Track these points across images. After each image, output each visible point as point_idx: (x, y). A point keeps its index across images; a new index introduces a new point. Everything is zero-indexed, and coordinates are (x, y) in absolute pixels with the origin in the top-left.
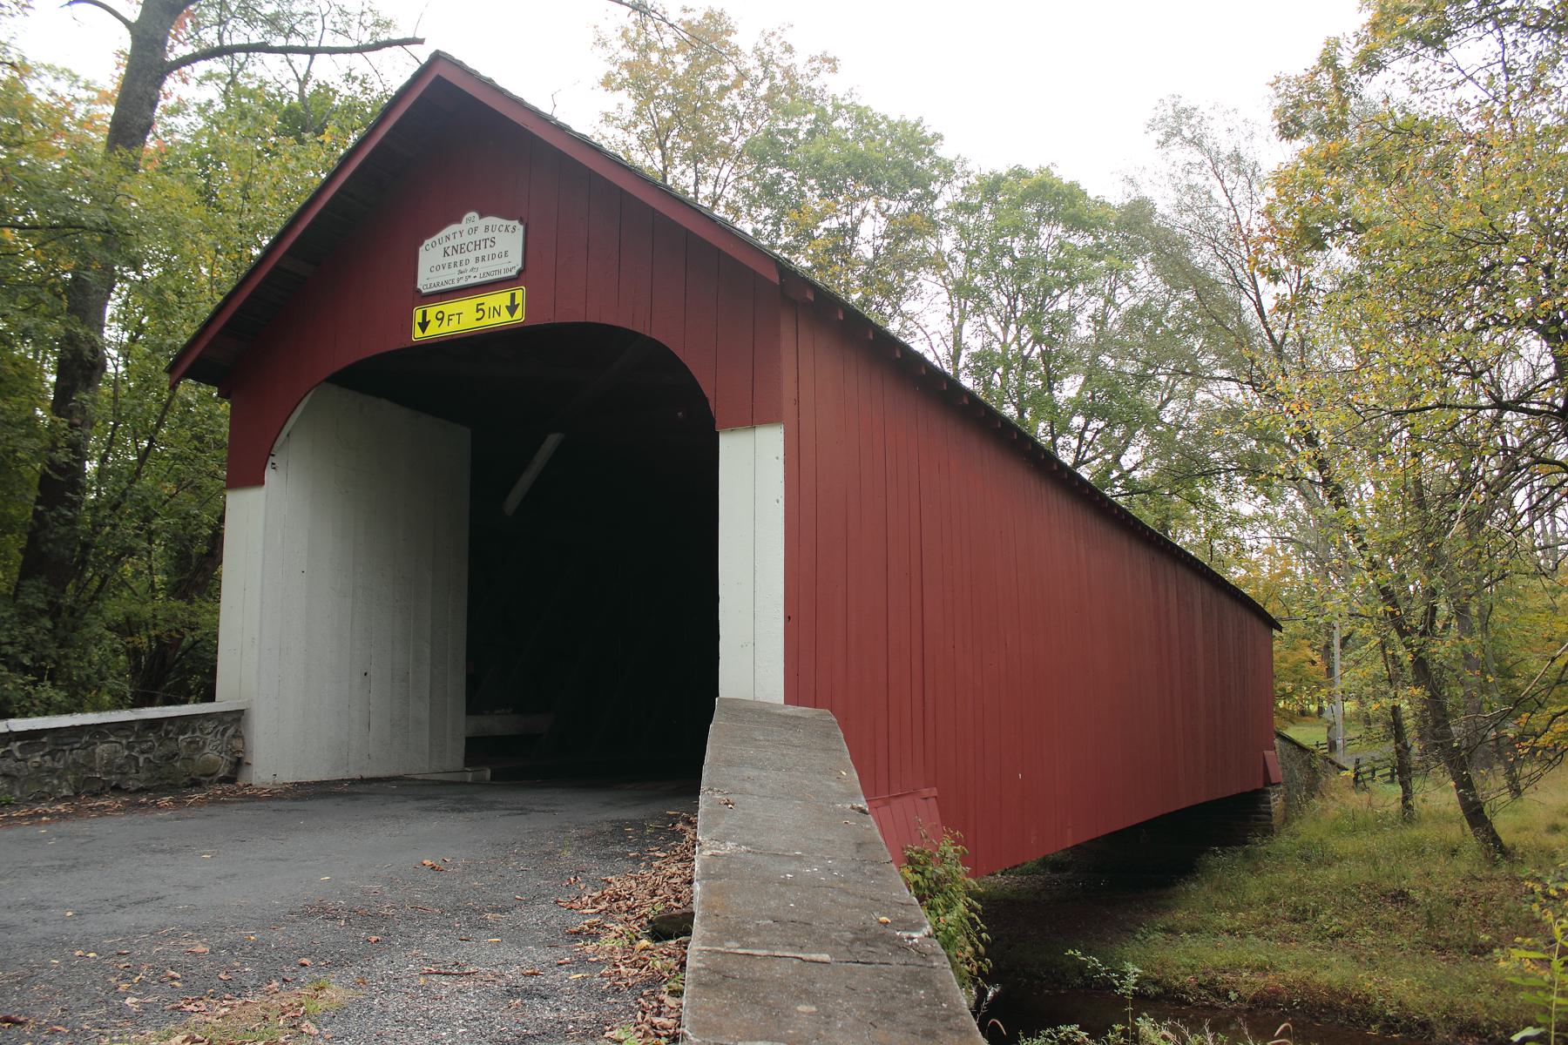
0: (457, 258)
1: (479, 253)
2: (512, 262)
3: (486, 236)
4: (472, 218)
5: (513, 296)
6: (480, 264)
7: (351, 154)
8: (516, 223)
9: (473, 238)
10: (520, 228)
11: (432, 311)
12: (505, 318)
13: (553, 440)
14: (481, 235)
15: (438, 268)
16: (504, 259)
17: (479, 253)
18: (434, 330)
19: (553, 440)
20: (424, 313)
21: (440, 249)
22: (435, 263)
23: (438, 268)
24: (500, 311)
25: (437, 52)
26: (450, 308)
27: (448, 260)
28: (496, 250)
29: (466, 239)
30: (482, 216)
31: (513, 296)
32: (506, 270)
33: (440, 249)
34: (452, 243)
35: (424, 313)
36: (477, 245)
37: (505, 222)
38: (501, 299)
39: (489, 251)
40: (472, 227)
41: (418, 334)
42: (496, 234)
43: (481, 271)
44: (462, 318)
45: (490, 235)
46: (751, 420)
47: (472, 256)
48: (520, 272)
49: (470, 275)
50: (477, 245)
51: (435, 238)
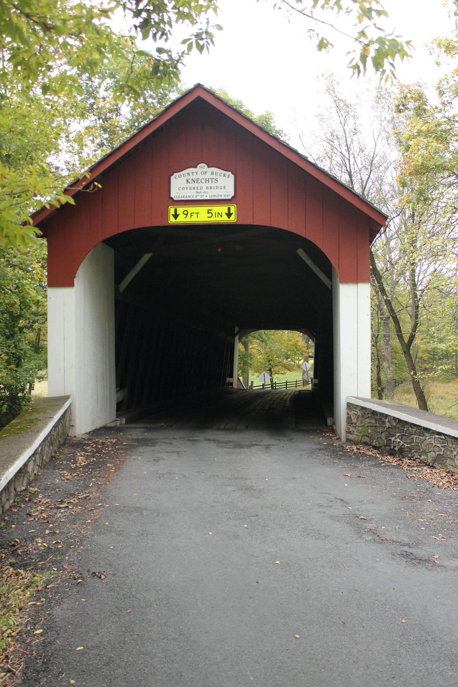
0: (195, 185)
1: (209, 185)
2: (229, 192)
3: (212, 177)
4: (202, 167)
5: (229, 209)
6: (209, 190)
7: (146, 126)
8: (230, 173)
9: (204, 176)
10: (232, 177)
11: (180, 210)
12: (224, 219)
13: (147, 257)
14: (208, 176)
15: (183, 188)
16: (223, 190)
17: (209, 185)
18: (182, 219)
19: (147, 257)
20: (176, 210)
21: (184, 180)
22: (181, 185)
23: (183, 188)
24: (219, 215)
25: (199, 84)
26: (191, 209)
27: (189, 185)
28: (218, 184)
29: (200, 176)
30: (209, 167)
31: (229, 209)
32: (225, 196)
33: (184, 180)
34: (191, 177)
35: (176, 210)
36: (207, 181)
37: (223, 172)
38: (223, 209)
39: (214, 185)
40: (202, 171)
41: (172, 220)
42: (218, 177)
43: (211, 194)
44: (201, 216)
45: (214, 176)
46: (356, 279)
47: (204, 185)
48: (233, 197)
49: (202, 194)
50: (207, 181)
51: (181, 173)
